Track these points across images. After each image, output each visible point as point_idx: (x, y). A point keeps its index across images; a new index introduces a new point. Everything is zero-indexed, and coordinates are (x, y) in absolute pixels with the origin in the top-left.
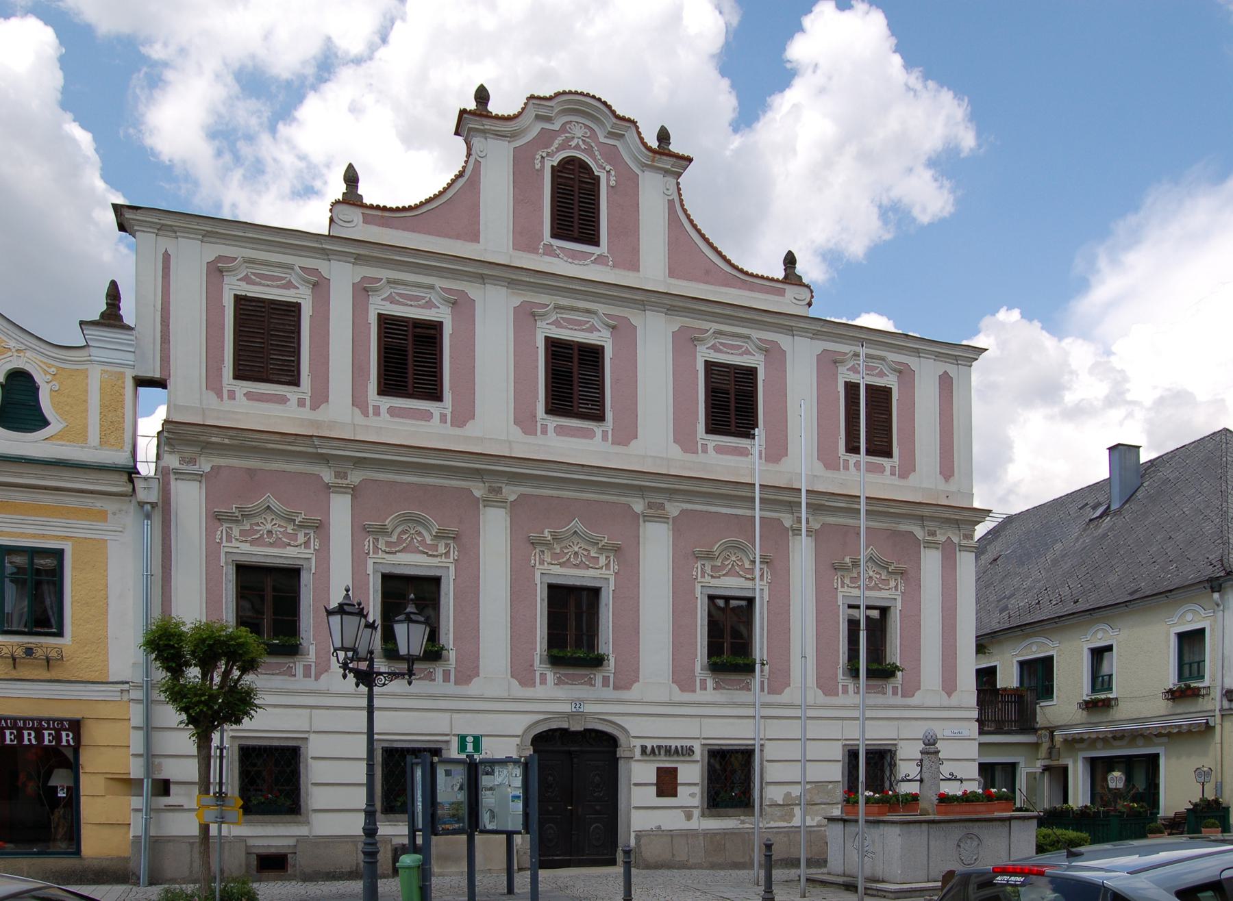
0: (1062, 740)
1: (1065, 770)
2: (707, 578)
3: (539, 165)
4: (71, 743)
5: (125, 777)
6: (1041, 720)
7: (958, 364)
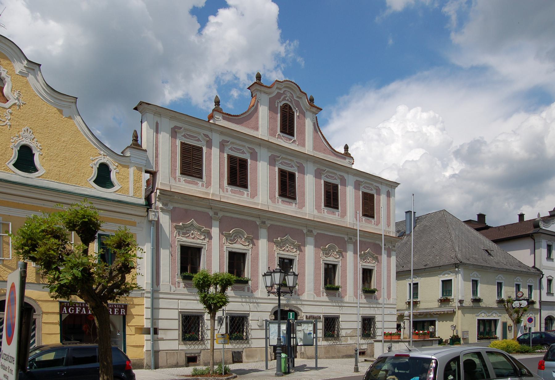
7: (382, 185)
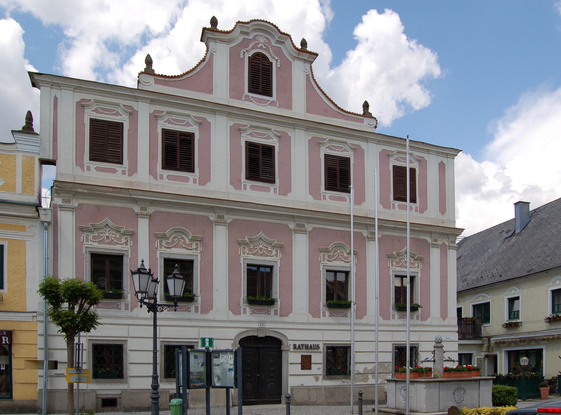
0: (494, 342)
1: (496, 357)
2: (326, 262)
3: (242, 56)
4: (7, 342)
5: (35, 359)
6: (484, 333)
7: (448, 158)
